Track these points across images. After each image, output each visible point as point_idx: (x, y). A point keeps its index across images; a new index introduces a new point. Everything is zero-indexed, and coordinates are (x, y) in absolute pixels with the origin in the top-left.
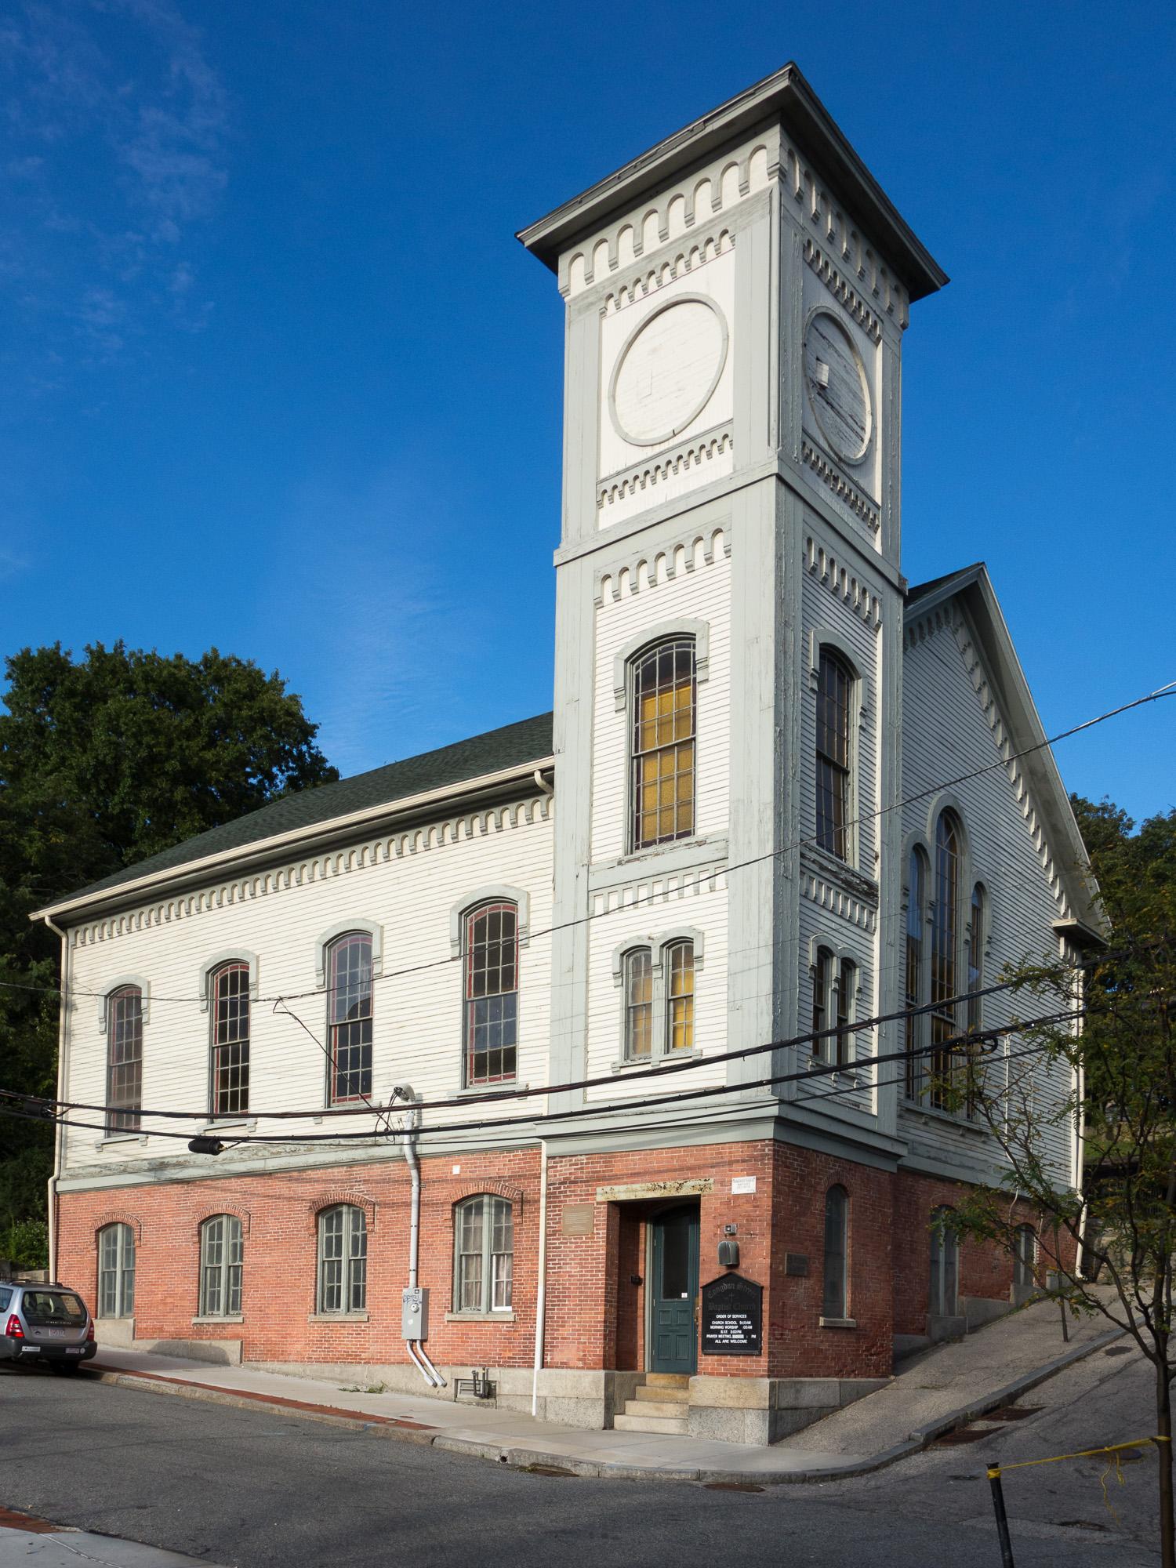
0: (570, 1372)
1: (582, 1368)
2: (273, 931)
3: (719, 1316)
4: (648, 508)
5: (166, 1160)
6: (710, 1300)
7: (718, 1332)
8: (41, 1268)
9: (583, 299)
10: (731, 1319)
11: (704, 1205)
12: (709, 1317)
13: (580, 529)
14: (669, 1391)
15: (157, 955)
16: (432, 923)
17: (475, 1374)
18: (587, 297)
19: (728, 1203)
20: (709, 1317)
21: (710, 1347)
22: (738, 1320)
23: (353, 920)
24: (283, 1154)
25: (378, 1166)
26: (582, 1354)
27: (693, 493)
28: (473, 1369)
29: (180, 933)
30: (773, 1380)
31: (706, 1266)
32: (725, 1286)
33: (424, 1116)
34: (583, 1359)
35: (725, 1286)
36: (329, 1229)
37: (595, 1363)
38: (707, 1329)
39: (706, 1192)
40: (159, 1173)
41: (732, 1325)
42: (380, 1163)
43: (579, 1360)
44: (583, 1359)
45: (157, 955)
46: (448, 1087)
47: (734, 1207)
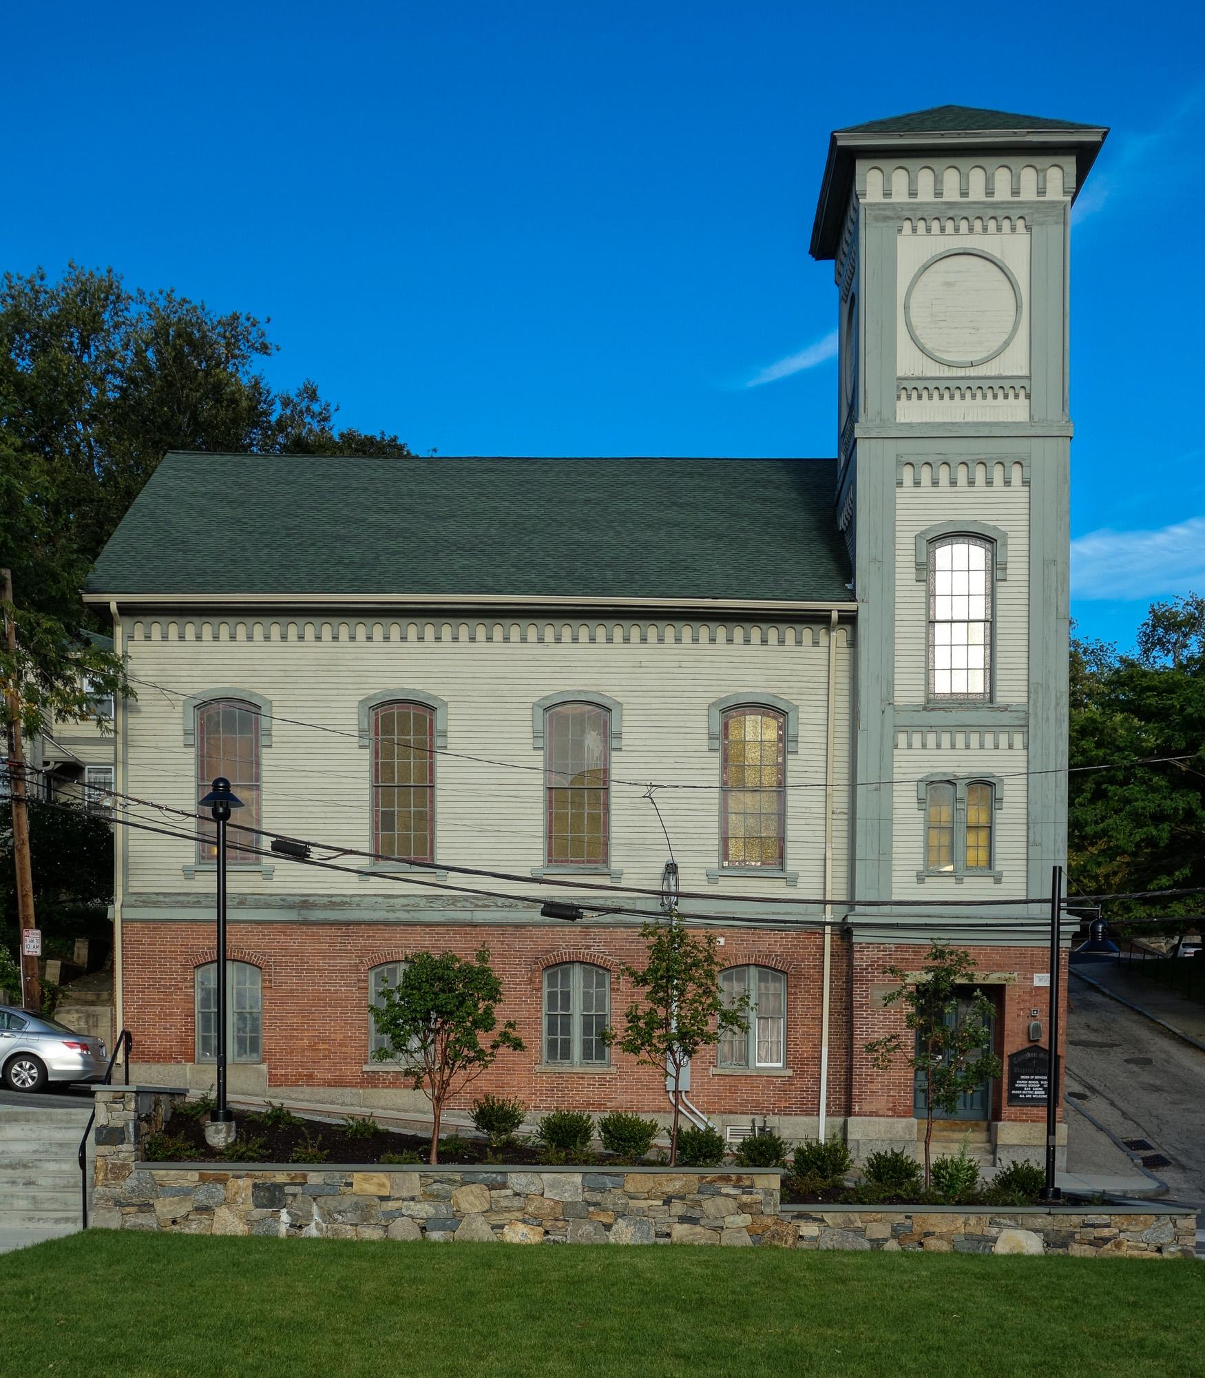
0: (883, 1119)
1: (892, 1116)
2: (469, 681)
3: (1022, 1077)
4: (954, 421)
5: (311, 899)
6: (1016, 1065)
7: (1022, 1089)
8: (103, 1003)
9: (880, 209)
10: (1034, 1080)
11: (1009, 993)
12: (1014, 1078)
13: (879, 413)
14: (945, 1133)
15: (282, 673)
16: (682, 712)
17: (753, 1121)
18: (884, 209)
19: (1030, 992)
20: (1014, 1078)
21: (1013, 1099)
22: (1040, 1080)
23: (586, 692)
24: (492, 908)
25: (623, 929)
26: (891, 1105)
27: (985, 424)
28: (752, 1117)
29: (320, 656)
30: (434, 1157)
31: (1010, 1039)
32: (1029, 1055)
33: (1024, 892)
34: (893, 1109)
35: (1029, 1055)
36: (552, 984)
37: (905, 1112)
38: (1012, 1086)
39: (1011, 983)
40: (304, 912)
41: (1035, 1084)
42: (625, 927)
43: (889, 1109)
44: (893, 1109)
45: (282, 673)
46: (708, 865)
47: (1035, 996)
